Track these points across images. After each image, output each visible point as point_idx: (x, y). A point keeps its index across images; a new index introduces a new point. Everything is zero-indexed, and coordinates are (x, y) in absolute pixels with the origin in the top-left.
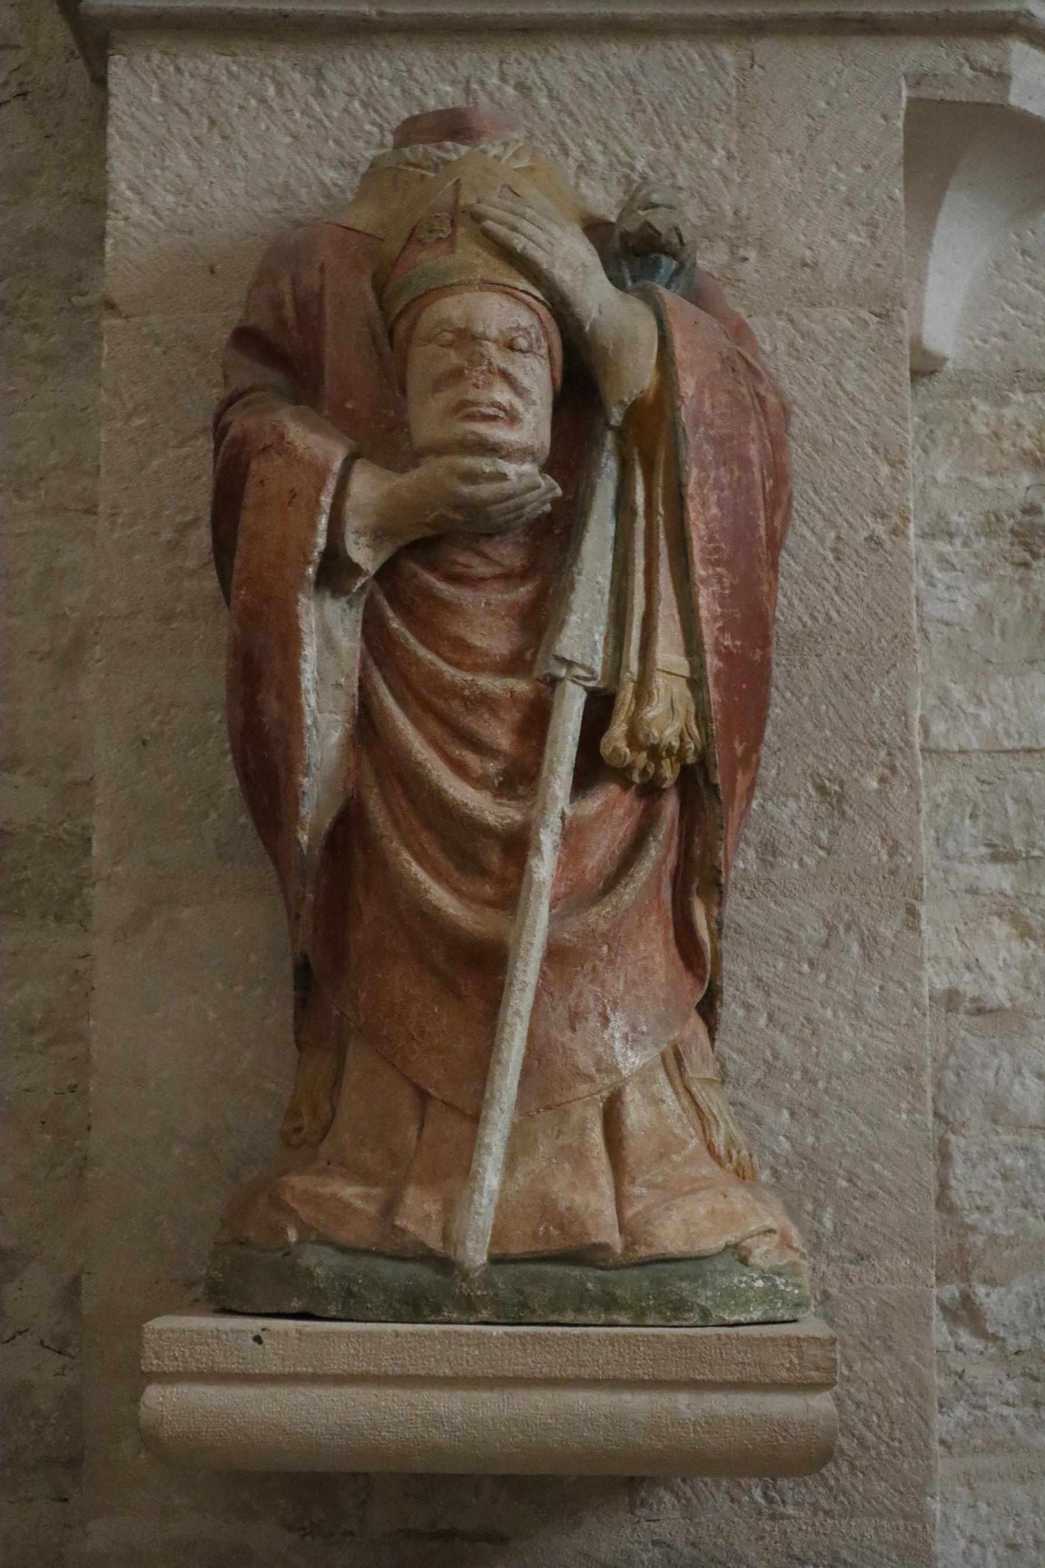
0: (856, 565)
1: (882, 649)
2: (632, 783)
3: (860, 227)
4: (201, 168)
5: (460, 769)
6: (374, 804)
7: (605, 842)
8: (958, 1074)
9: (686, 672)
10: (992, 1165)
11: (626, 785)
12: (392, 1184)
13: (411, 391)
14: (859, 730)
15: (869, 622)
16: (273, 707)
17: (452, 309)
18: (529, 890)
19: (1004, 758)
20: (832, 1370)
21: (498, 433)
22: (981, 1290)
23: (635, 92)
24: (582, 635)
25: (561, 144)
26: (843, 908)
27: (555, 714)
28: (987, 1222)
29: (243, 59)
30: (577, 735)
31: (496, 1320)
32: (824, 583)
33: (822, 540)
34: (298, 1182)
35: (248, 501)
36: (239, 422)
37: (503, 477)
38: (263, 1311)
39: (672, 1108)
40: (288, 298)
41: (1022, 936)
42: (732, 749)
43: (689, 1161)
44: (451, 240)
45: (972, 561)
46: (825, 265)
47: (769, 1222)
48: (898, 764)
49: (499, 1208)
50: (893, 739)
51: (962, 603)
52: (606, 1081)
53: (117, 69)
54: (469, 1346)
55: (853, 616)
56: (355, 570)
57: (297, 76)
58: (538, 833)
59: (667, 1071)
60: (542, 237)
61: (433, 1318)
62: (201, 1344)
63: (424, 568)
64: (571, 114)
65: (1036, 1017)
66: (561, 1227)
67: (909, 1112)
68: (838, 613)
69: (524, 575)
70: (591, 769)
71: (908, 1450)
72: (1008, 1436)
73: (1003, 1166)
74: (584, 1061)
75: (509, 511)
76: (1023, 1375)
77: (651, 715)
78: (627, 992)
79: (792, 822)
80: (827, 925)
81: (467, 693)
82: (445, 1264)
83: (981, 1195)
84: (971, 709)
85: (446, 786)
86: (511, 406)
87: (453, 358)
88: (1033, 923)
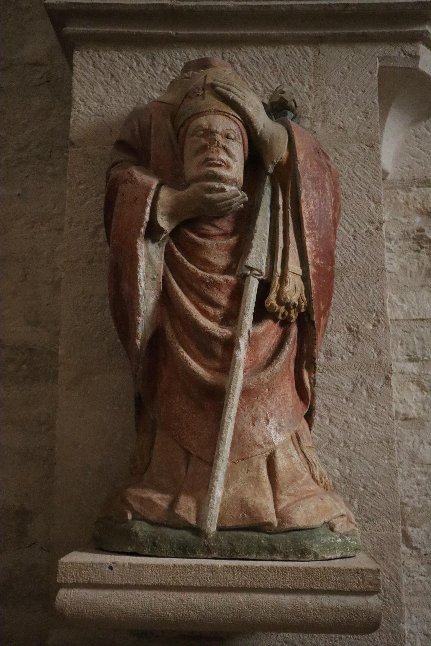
0: (362, 241)
1: (373, 274)
2: (278, 320)
3: (361, 113)
4: (107, 92)
5: (205, 314)
6: (168, 328)
7: (267, 345)
8: (398, 444)
9: (301, 273)
10: (413, 479)
11: (275, 320)
12: (175, 492)
13: (185, 158)
14: (364, 306)
15: (368, 263)
16: (126, 286)
17: (203, 121)
18: (235, 364)
19: (413, 322)
20: (377, 585)
21: (222, 171)
22: (410, 529)
23: (274, 64)
24: (257, 257)
25: (247, 79)
26: (359, 377)
27: (245, 290)
28: (412, 502)
29: (124, 52)
30: (255, 299)
31: (220, 557)
32: (350, 249)
33: (348, 232)
34: (134, 492)
35: (118, 201)
36: (114, 173)
37: (223, 190)
38: (116, 550)
39: (297, 459)
40: (137, 128)
41: (422, 390)
42: (319, 307)
43: (306, 483)
44: (203, 96)
45: (398, 249)
46: (348, 128)
47: (343, 511)
48: (380, 319)
49: (221, 505)
50: (378, 309)
51: (395, 265)
52: (268, 448)
53: (77, 56)
54: (208, 572)
55: (361, 261)
56: (162, 230)
57: (145, 59)
58: (238, 340)
59: (293, 443)
60: (240, 94)
61: (191, 556)
62: (85, 570)
63: (190, 232)
64: (249, 72)
65: (428, 421)
66: (250, 514)
67: (388, 460)
68: (355, 260)
69: (232, 234)
70: (262, 313)
71: (392, 602)
72: (423, 589)
73: (417, 479)
74: (259, 439)
75: (226, 206)
76: (428, 563)
77: (287, 290)
78: (276, 409)
79: (338, 342)
80: (353, 383)
81: (208, 281)
82: (198, 531)
83: (409, 491)
84: (400, 304)
85: (199, 320)
86: (227, 161)
87: (203, 141)
88: (425, 385)
